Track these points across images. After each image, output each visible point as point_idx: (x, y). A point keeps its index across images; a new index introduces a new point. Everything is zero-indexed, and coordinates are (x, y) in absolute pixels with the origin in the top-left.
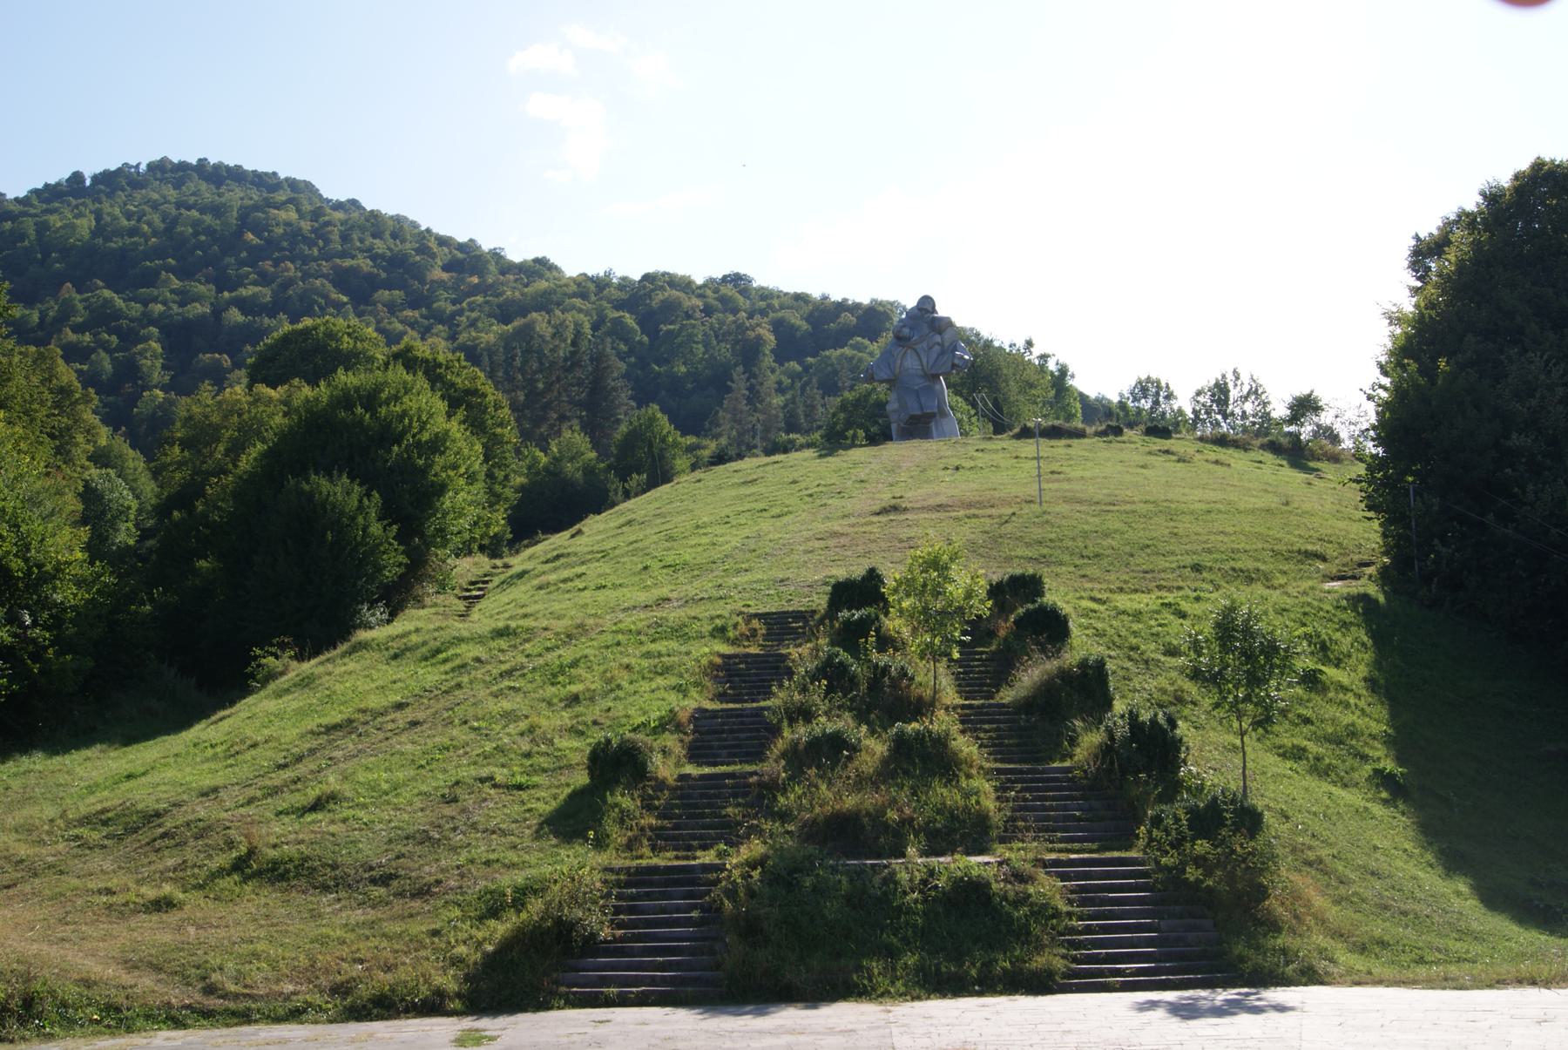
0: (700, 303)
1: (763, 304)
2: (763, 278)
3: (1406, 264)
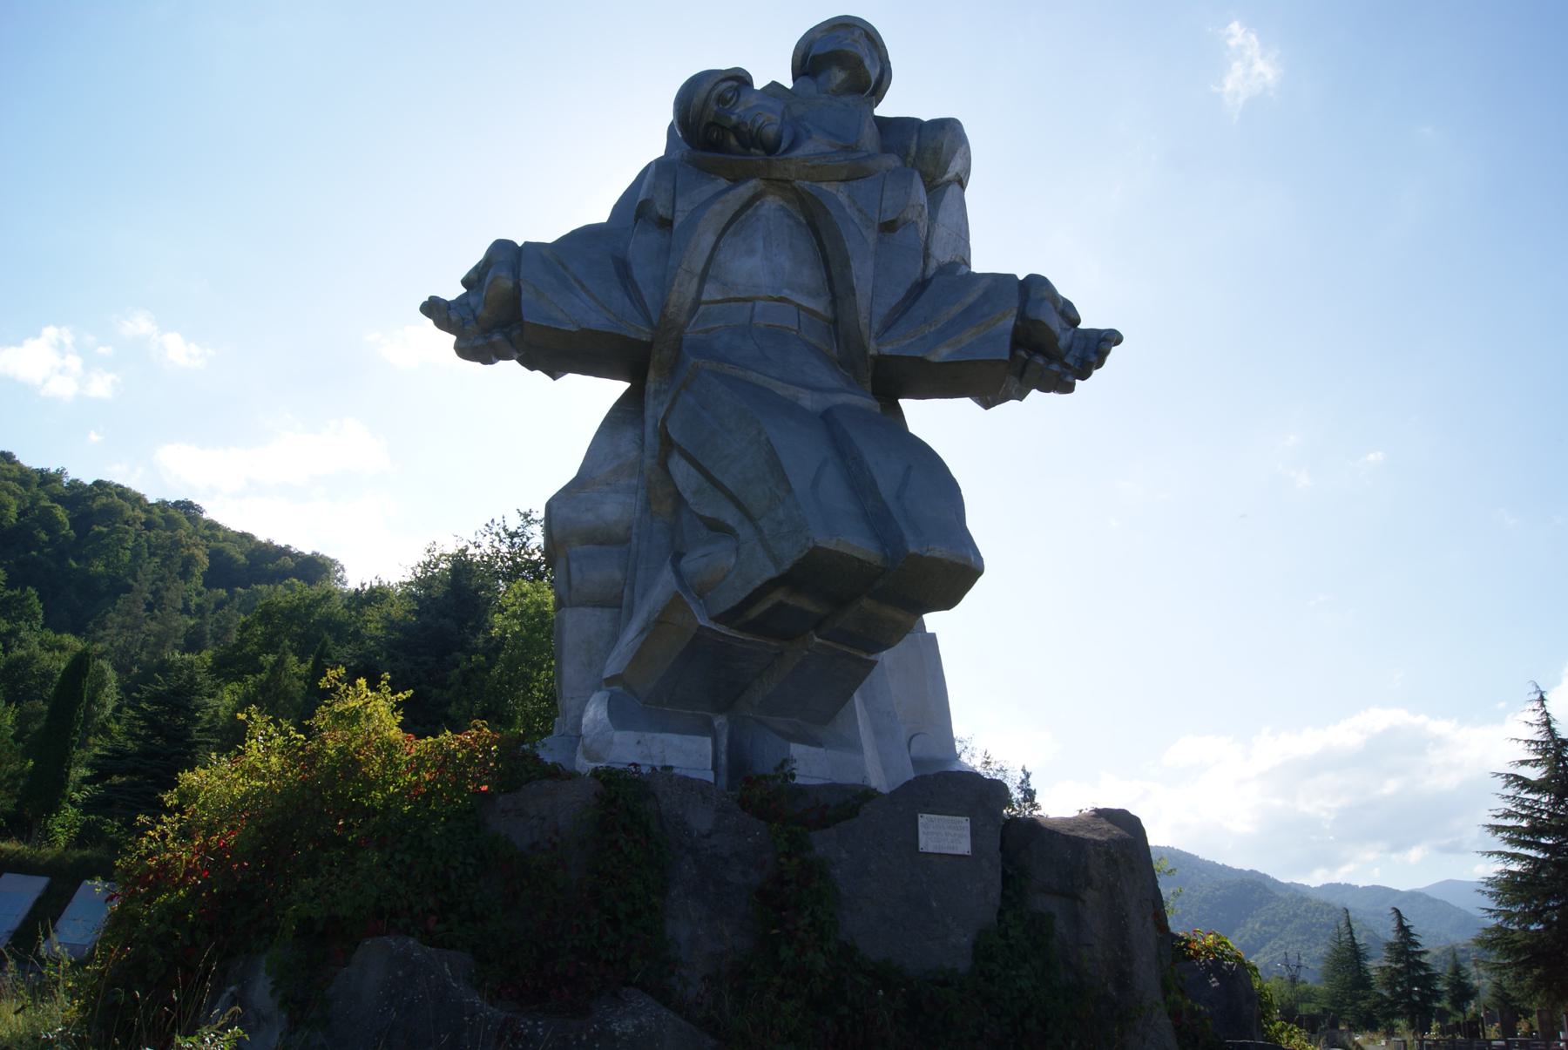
0: (143, 516)
1: (207, 533)
2: (213, 512)
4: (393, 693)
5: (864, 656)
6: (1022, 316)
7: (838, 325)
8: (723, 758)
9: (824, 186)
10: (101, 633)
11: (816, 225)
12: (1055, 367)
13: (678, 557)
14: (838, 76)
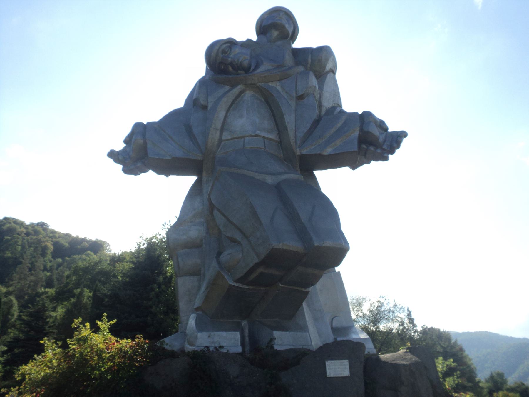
0: (25, 231)
1: (51, 235)
2: (54, 226)
4: (108, 322)
5: (303, 290)
6: (361, 130)
7: (282, 142)
8: (247, 339)
9: (270, 84)
10: (11, 283)
11: (269, 102)
12: (379, 151)
13: (219, 254)
14: (275, 33)
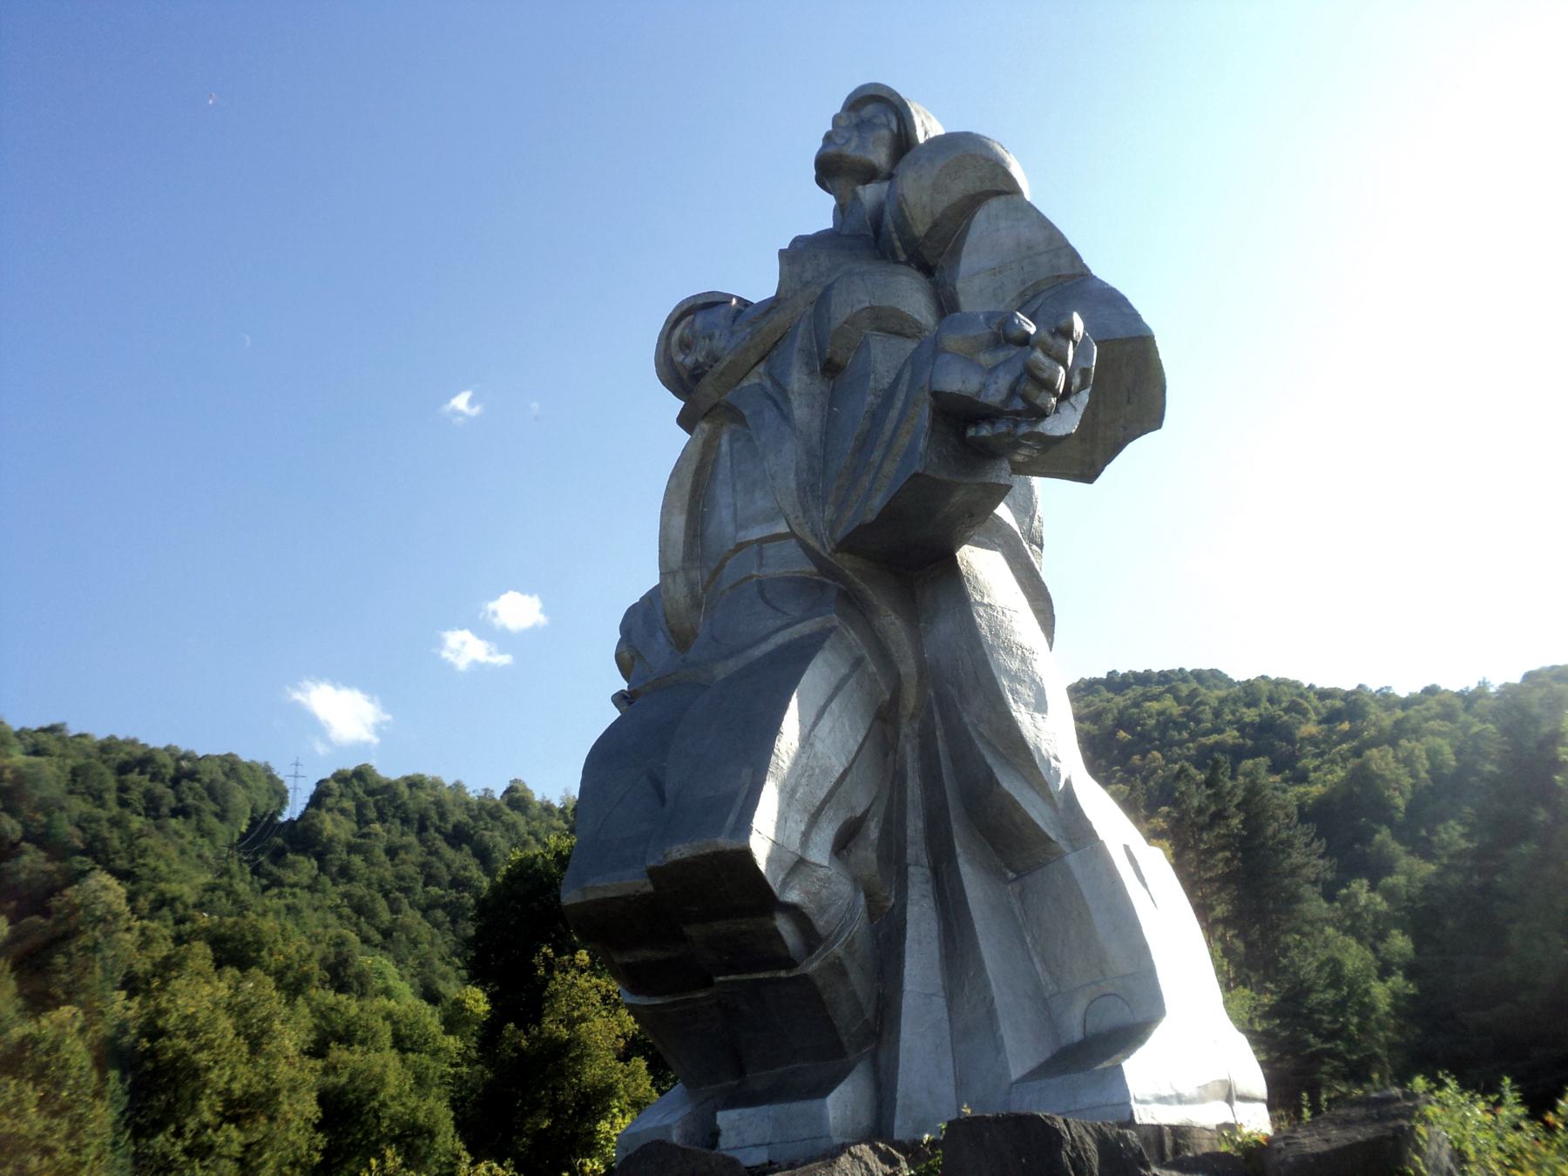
3: (272, 765)
